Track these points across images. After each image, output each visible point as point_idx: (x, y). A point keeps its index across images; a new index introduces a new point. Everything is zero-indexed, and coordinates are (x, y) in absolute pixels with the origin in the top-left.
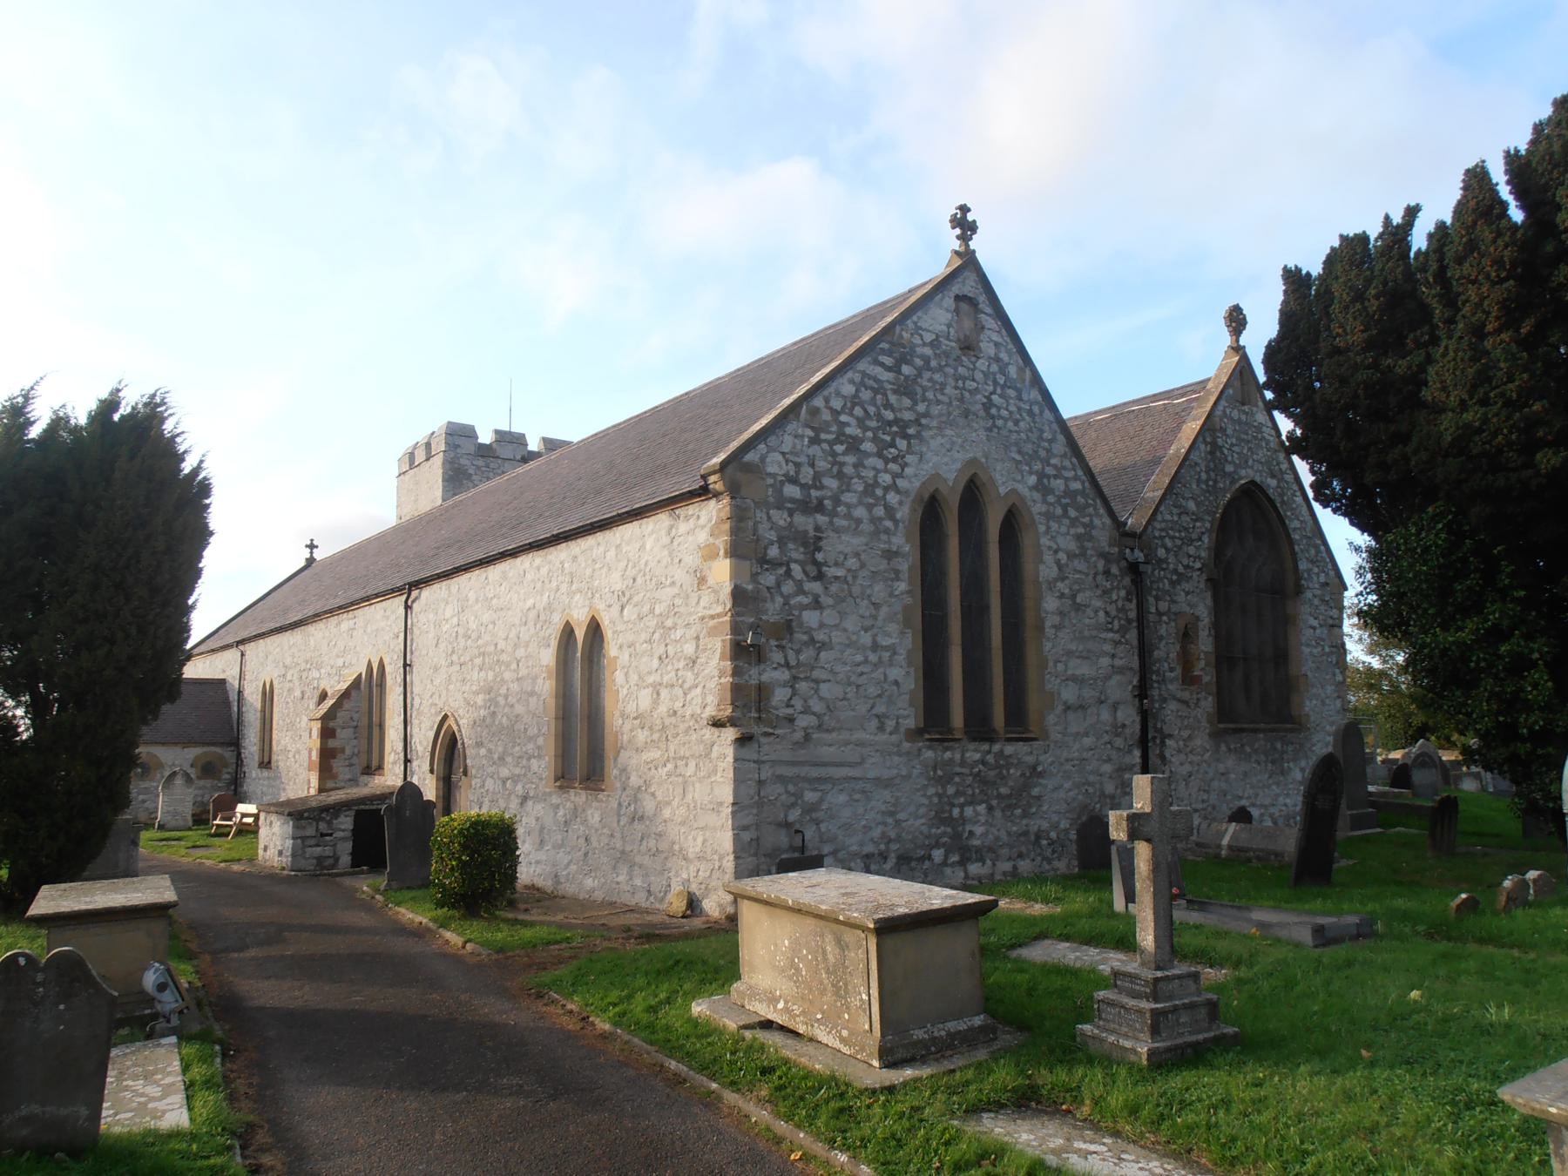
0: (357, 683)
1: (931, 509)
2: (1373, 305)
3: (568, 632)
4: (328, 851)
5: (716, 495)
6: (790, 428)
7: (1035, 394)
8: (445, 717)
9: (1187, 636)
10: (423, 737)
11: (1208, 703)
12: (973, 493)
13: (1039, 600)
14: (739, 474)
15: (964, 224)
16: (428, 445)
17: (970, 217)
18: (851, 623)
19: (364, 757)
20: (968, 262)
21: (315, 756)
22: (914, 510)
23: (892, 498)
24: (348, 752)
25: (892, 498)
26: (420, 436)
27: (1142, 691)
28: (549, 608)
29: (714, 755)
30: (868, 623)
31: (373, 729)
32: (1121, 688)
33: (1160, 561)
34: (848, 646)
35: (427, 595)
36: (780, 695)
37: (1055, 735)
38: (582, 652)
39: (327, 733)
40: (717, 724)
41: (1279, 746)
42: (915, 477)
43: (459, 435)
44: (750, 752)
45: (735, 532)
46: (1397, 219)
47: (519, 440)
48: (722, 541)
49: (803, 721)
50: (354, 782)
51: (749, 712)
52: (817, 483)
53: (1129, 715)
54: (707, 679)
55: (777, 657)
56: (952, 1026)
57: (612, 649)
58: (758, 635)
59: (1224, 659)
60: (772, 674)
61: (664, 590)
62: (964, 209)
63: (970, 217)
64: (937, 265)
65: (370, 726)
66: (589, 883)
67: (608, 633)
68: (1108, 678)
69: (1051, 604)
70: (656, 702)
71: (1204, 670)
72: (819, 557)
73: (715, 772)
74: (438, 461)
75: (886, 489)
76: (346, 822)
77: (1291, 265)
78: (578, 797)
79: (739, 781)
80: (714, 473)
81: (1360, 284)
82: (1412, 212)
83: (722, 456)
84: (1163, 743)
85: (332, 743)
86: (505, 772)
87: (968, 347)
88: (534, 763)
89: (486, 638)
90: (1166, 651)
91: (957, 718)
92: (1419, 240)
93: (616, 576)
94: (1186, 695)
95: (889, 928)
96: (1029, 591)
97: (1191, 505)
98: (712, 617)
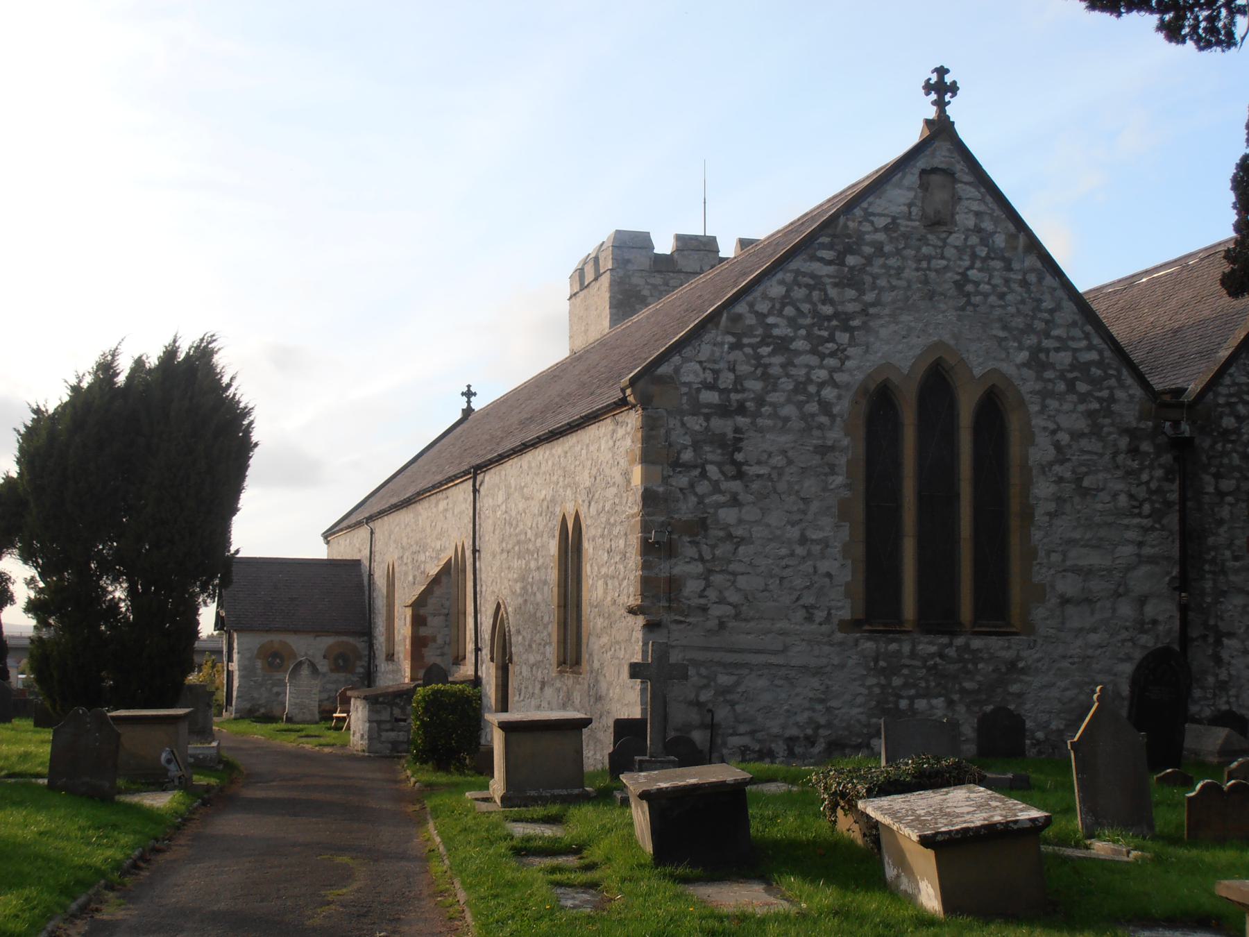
1: (880, 402)
12: (938, 381)
17: (948, 79)
30: (796, 517)
40: (632, 611)
42: (859, 367)
49: (716, 611)
55: (691, 552)
60: (685, 567)
62: (942, 71)
63: (948, 79)
64: (911, 135)
68: (1130, 568)
69: (1043, 489)
74: (605, 280)
75: (822, 385)
78: (569, 680)
80: (627, 387)
84: (1218, 642)
85: (424, 631)
91: (966, 611)
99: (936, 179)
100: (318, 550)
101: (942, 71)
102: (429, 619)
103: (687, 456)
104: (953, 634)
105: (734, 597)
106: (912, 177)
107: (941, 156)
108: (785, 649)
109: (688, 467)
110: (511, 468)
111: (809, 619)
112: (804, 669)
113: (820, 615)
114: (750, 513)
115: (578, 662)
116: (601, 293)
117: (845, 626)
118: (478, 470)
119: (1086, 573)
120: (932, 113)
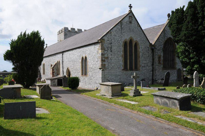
0: (56, 64)
1: (125, 43)
2: (177, 18)
3: (83, 58)
4: (55, 84)
5: (100, 43)
6: (108, 34)
7: (139, 28)
8: (68, 68)
9: (159, 58)
10: (65, 70)
11: (162, 66)
12: (131, 41)
13: (139, 54)
14: (101, 41)
15: (130, 7)
16: (62, 30)
17: (131, 6)
18: (115, 57)
19: (58, 73)
20: (131, 12)
21: (52, 73)
22: (123, 43)
23: (121, 42)
24: (56, 72)
25: (121, 42)
26: (61, 29)
27: (153, 65)
28: (80, 55)
29: (100, 72)
30: (117, 57)
31: (58, 70)
32: (150, 64)
33: (156, 48)
34: (115, 60)
35: (65, 53)
36: (107, 65)
37: (141, 70)
38: (84, 61)
39: (53, 70)
40: (100, 69)
41: (172, 71)
42: (123, 39)
43: (66, 29)
44: (103, 72)
45: (101, 47)
46: (182, 7)
47: (74, 29)
48: (100, 48)
49: (109, 68)
50: (56, 76)
51: (103, 68)
52: (111, 41)
53: (151, 68)
54: (99, 64)
55: (107, 61)
56: (118, 94)
57: (88, 60)
58: (104, 59)
59: (164, 61)
60: (106, 63)
61: (94, 54)
62: (130, 5)
63: (131, 6)
64: (127, 12)
65: (58, 69)
66: (86, 87)
67: (87, 58)
68: (148, 63)
69: (141, 54)
70: (93, 66)
71: (162, 62)
72: (112, 49)
73: (99, 74)
74: (63, 33)
75: (120, 41)
76: (56, 81)
77: (173, 11)
78: (84, 77)
79: (102, 75)
80: (99, 40)
81: (176, 15)
82: (184, 6)
83: (100, 38)
84: (155, 71)
85: (54, 71)
86: (76, 74)
87: (131, 22)
88: (79, 73)
89: (73, 58)
90: (156, 59)
91: (128, 68)
92: (185, 9)
93: (88, 51)
94: (159, 65)
95: (112, 86)
96: (138, 53)
97: (161, 41)
98: (99, 57)
99: (130, 17)
100: (43, 63)
101: (130, 5)
102: (54, 70)
103: (106, 49)
104: (133, 71)
105: (111, 67)
106: (128, 17)
107: (131, 15)
108: (117, 73)
109: (106, 50)
110: (67, 53)
111: (119, 69)
112: (119, 75)
113: (120, 69)
114: (113, 56)
115: (44, 74)
116: (63, 34)
117: (122, 70)
118: (63, 52)
119: (145, 63)
120: (129, 9)
